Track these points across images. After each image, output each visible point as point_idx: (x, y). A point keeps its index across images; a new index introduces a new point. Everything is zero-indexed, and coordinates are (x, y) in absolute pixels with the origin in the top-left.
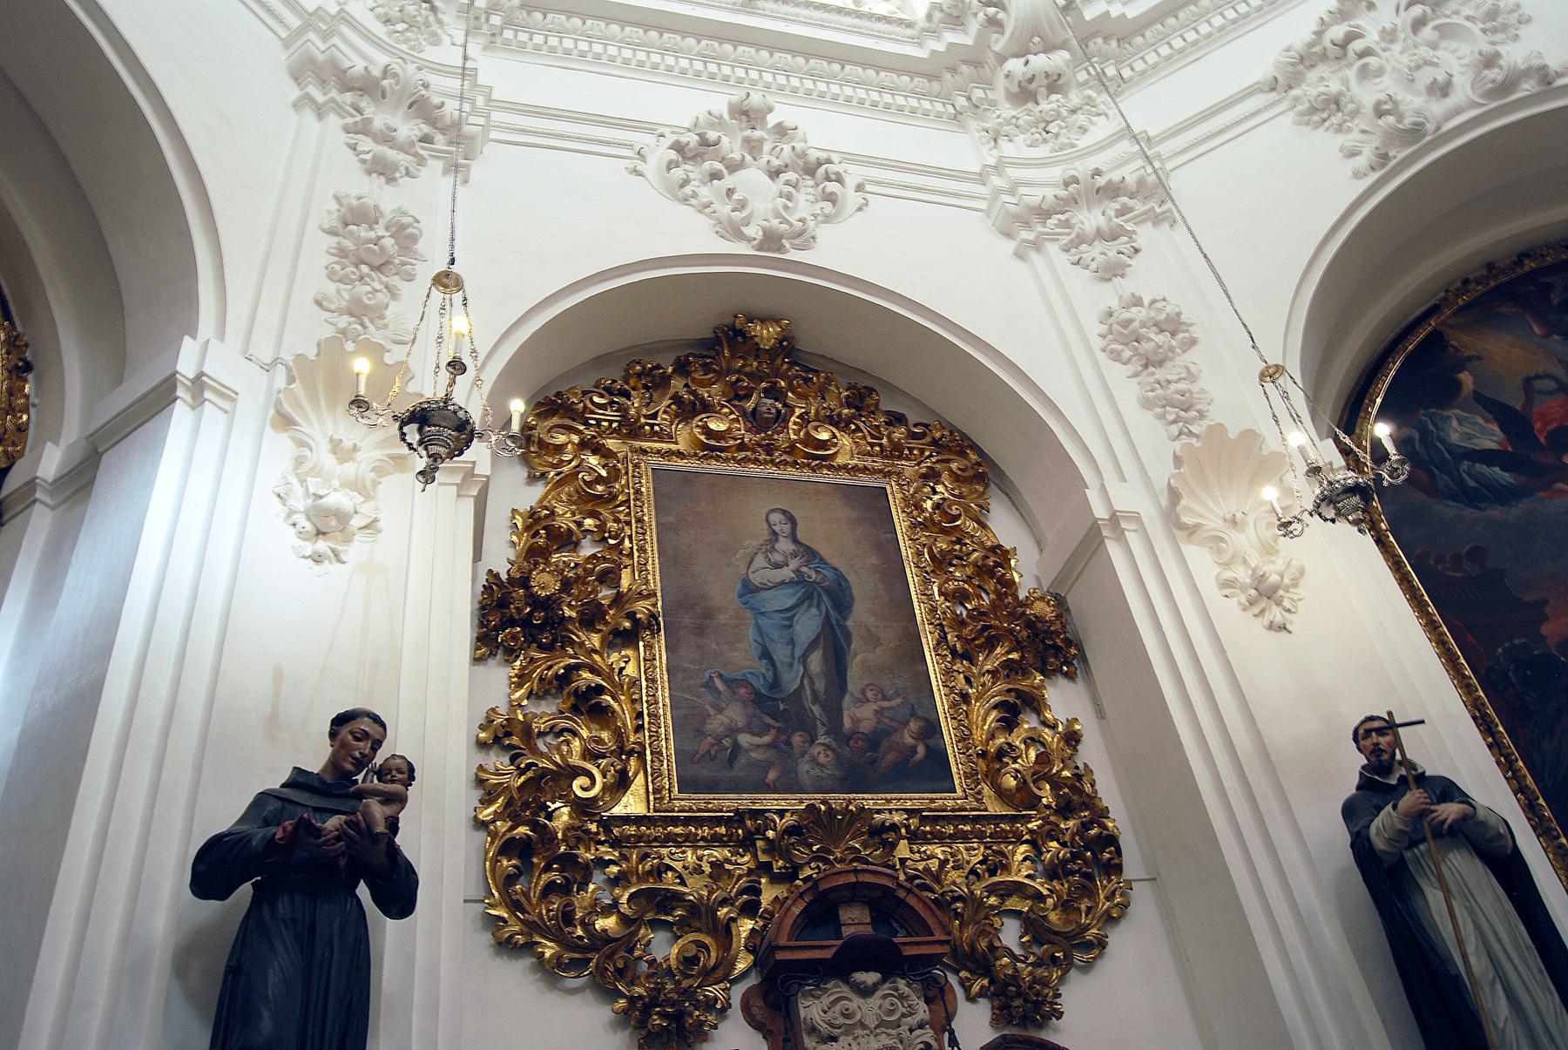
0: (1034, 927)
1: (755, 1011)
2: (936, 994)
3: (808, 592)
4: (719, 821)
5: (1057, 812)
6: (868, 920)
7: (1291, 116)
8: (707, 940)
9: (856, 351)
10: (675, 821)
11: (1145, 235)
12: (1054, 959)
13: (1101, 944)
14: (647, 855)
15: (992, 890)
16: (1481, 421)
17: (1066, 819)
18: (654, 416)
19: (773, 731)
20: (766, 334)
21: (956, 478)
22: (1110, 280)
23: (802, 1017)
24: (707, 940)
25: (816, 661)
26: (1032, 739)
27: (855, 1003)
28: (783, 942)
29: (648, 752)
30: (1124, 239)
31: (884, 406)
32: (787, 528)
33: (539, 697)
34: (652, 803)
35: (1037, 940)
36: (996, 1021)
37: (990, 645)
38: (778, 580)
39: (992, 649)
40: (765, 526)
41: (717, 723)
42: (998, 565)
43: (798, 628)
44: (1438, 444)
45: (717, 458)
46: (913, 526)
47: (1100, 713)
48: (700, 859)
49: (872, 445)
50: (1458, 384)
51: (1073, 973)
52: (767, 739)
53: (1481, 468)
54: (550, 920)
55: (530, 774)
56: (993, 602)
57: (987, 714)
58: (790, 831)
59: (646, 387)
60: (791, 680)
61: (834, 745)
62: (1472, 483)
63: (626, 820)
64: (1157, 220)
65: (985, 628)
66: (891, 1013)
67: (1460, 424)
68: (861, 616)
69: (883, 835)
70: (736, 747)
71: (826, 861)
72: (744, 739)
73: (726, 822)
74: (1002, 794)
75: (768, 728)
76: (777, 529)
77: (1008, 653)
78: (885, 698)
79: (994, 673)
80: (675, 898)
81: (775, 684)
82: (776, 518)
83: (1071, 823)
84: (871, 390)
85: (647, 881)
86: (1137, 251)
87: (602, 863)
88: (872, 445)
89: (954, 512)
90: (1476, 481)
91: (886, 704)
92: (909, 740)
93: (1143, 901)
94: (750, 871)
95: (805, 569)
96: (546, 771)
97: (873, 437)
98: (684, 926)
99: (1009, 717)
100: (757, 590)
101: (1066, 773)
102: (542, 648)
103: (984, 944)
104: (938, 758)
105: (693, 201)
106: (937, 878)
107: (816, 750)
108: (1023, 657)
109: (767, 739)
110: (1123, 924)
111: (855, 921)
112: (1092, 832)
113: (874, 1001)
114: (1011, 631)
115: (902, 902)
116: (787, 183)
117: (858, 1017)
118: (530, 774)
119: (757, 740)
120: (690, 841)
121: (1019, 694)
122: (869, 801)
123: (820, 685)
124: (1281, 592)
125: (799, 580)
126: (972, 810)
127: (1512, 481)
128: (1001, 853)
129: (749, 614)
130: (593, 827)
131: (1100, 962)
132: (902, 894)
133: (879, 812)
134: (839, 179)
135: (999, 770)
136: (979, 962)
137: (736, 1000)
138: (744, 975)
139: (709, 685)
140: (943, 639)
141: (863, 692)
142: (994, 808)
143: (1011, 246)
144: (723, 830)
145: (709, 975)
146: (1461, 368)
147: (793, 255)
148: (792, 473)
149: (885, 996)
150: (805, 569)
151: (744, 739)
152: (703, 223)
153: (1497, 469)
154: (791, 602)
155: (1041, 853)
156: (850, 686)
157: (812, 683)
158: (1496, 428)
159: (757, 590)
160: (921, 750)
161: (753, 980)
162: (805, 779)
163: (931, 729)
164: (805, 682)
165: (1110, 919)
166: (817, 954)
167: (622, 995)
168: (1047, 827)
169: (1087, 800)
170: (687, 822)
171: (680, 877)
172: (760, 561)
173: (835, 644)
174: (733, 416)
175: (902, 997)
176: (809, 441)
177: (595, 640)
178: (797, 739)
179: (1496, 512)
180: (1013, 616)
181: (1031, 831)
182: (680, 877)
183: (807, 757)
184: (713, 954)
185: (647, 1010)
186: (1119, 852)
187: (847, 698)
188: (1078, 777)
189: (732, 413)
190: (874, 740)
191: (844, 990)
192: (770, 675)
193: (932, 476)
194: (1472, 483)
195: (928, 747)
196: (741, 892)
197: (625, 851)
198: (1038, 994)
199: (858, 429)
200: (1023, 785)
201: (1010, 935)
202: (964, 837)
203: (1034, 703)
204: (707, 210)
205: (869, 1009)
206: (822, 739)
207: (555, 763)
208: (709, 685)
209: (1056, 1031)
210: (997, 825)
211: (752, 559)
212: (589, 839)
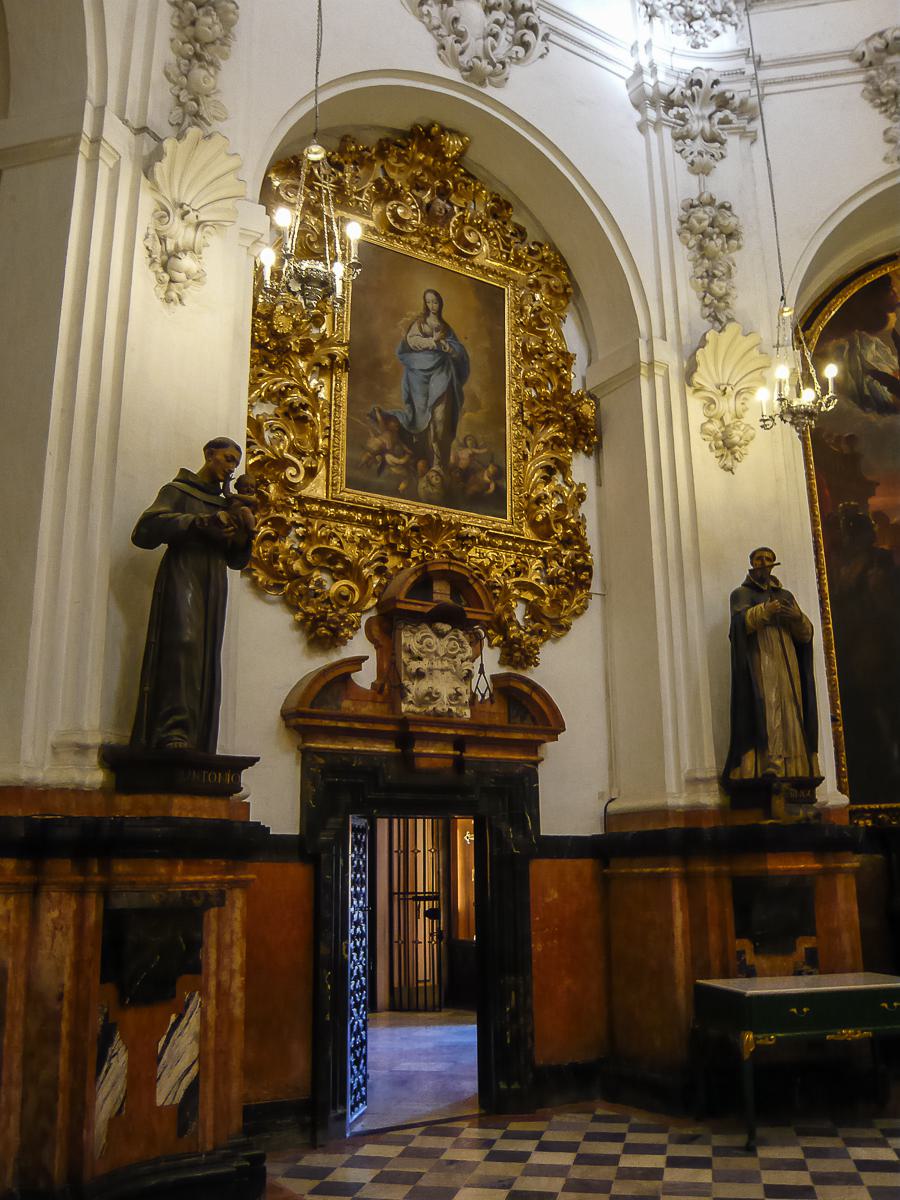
0: (534, 611)
1: (374, 632)
2: (476, 641)
3: (443, 360)
4: (369, 512)
5: (560, 542)
6: (449, 592)
7: (863, 86)
8: (354, 586)
9: (508, 174)
10: (344, 507)
11: (733, 143)
12: (541, 632)
13: (567, 628)
14: (323, 525)
15: (517, 585)
16: (890, 352)
17: (566, 549)
18: (360, 194)
19: (407, 456)
20: (453, 145)
21: (551, 291)
22: (698, 174)
23: (403, 642)
24: (354, 586)
25: (440, 411)
26: (557, 492)
27: (434, 640)
28: (402, 597)
29: (331, 456)
30: (717, 145)
31: (515, 219)
32: (436, 306)
33: (263, 401)
34: (330, 492)
35: (534, 619)
36: (502, 663)
37: (547, 423)
38: (425, 346)
39: (547, 426)
40: (422, 301)
41: (374, 443)
42: (564, 367)
43: (432, 385)
44: (858, 358)
45: (398, 241)
46: (518, 325)
47: (599, 483)
48: (353, 533)
49: (502, 253)
50: (886, 320)
51: (548, 642)
52: (402, 461)
53: (877, 384)
54: (265, 557)
55: (258, 458)
56: (554, 394)
57: (536, 470)
58: (414, 529)
59: (355, 163)
60: (423, 422)
61: (442, 473)
62: (867, 392)
63: (314, 501)
64: (743, 133)
65: (547, 412)
66: (453, 649)
67: (877, 349)
68: (473, 385)
69: (463, 540)
70: (384, 463)
71: (429, 550)
72: (389, 458)
73: (374, 513)
74: (533, 524)
75: (404, 453)
76: (430, 306)
77: (558, 431)
78: (477, 447)
79: (546, 444)
80: (338, 557)
81: (413, 423)
82: (430, 297)
83: (568, 552)
84: (508, 206)
85: (322, 543)
86: (723, 157)
87: (296, 525)
88: (502, 253)
89: (546, 321)
90: (870, 391)
91: (477, 451)
92: (486, 478)
93: (595, 603)
94: (382, 547)
95: (443, 342)
96: (269, 459)
97: (505, 247)
98: (342, 574)
99: (549, 473)
100: (411, 351)
101: (572, 521)
102: (272, 367)
103: (506, 617)
104: (501, 493)
105: (426, 20)
106: (487, 570)
107: (431, 474)
108: (565, 437)
109: (402, 461)
110: (581, 618)
111: (441, 593)
112: (579, 561)
113: (445, 642)
114: (563, 419)
115: (470, 586)
116: (497, 22)
117: (434, 649)
118: (258, 458)
119: (396, 460)
120: (350, 520)
121: (557, 461)
122: (454, 515)
123: (440, 428)
124: (737, 448)
125: (437, 350)
126: (516, 534)
127: (891, 400)
128: (525, 563)
129: (404, 368)
130: (292, 500)
131: (564, 638)
132: (471, 581)
133: (465, 526)
134: (533, 28)
135: (535, 510)
136: (501, 626)
137: (363, 624)
138: (369, 610)
139: (373, 417)
140: (520, 413)
141: (465, 440)
142: (528, 534)
143: (637, 117)
144: (369, 518)
145: (353, 608)
146: (892, 310)
147: (489, 91)
148: (446, 264)
149: (451, 639)
150: (443, 342)
151: (389, 458)
152: (429, 42)
153: (886, 388)
154: (430, 365)
155: (547, 567)
156: (458, 434)
157: (435, 428)
158: (896, 359)
159: (411, 351)
160: (492, 487)
161: (373, 614)
162: (421, 492)
163: (500, 474)
164: (432, 426)
165: (576, 615)
166: (419, 608)
167: (302, 611)
168: (555, 552)
169: (580, 538)
170: (350, 509)
171: (340, 542)
172: (415, 328)
173: (453, 399)
174: (413, 207)
175: (461, 642)
176: (461, 239)
177: (302, 364)
178: (420, 464)
179: (873, 417)
180: (566, 409)
181: (545, 552)
182: (340, 542)
183: (425, 478)
184: (357, 594)
185: (316, 622)
186: (591, 576)
187: (454, 443)
188: (579, 523)
189: (414, 204)
190: (467, 474)
191: (429, 632)
192: (410, 416)
193: (536, 286)
194: (867, 392)
195: (497, 487)
196: (376, 560)
197: (310, 520)
198: (531, 652)
199: (495, 237)
200: (546, 519)
201: (520, 612)
202: (507, 548)
203: (563, 467)
204: (435, 32)
205: (442, 646)
206: (435, 468)
207: (276, 455)
208: (373, 417)
209: (532, 672)
210: (527, 546)
211: (410, 327)
212: (287, 507)
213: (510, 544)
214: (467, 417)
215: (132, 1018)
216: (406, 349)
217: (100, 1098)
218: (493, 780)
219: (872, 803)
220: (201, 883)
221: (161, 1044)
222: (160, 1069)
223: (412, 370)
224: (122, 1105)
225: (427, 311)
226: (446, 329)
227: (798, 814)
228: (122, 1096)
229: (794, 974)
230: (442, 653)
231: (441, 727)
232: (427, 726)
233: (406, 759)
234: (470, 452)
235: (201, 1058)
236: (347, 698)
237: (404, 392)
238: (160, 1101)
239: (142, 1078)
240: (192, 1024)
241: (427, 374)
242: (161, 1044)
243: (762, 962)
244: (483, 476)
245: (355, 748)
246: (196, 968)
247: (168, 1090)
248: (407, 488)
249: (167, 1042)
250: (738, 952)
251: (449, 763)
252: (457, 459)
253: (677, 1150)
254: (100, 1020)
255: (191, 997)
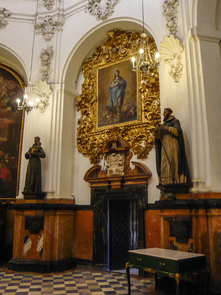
6: (116, 145)
30: (45, 29)
52: (110, 116)
60: (115, 104)
61: (120, 115)
68: (128, 89)
70: (106, 118)
75: (111, 114)
76: (116, 75)
82: (116, 72)
91: (129, 105)
95: (119, 82)
139: (104, 109)
150: (119, 82)
156: (124, 103)
157: (118, 104)
160: (133, 113)
183: (116, 118)
187: (123, 106)
190: (126, 113)
206: (118, 114)
208: (104, 109)
213: (131, 127)
214: (126, 97)
215: (32, 236)
216: (111, 88)
217: (25, 248)
218: (135, 190)
219: (13, 198)
220: (31, 214)
221: (38, 241)
222: (37, 245)
223: (112, 93)
224: (30, 249)
225: (116, 76)
226: (120, 78)
227: (165, 197)
228: (30, 248)
229: (188, 252)
230: (114, 160)
231: (113, 178)
232: (109, 179)
233: (110, 187)
234: (127, 106)
235: (43, 244)
236: (99, 174)
237: (110, 99)
238: (37, 250)
239: (34, 245)
240: (42, 238)
241: (116, 92)
242: (38, 241)
243: (180, 246)
244: (130, 111)
245: (99, 185)
246: (43, 229)
247: (39, 249)
248: (111, 122)
249: (39, 241)
250: (170, 241)
251: (120, 187)
252: (124, 110)
253: (44, 279)
254: (25, 235)
255: (42, 234)
